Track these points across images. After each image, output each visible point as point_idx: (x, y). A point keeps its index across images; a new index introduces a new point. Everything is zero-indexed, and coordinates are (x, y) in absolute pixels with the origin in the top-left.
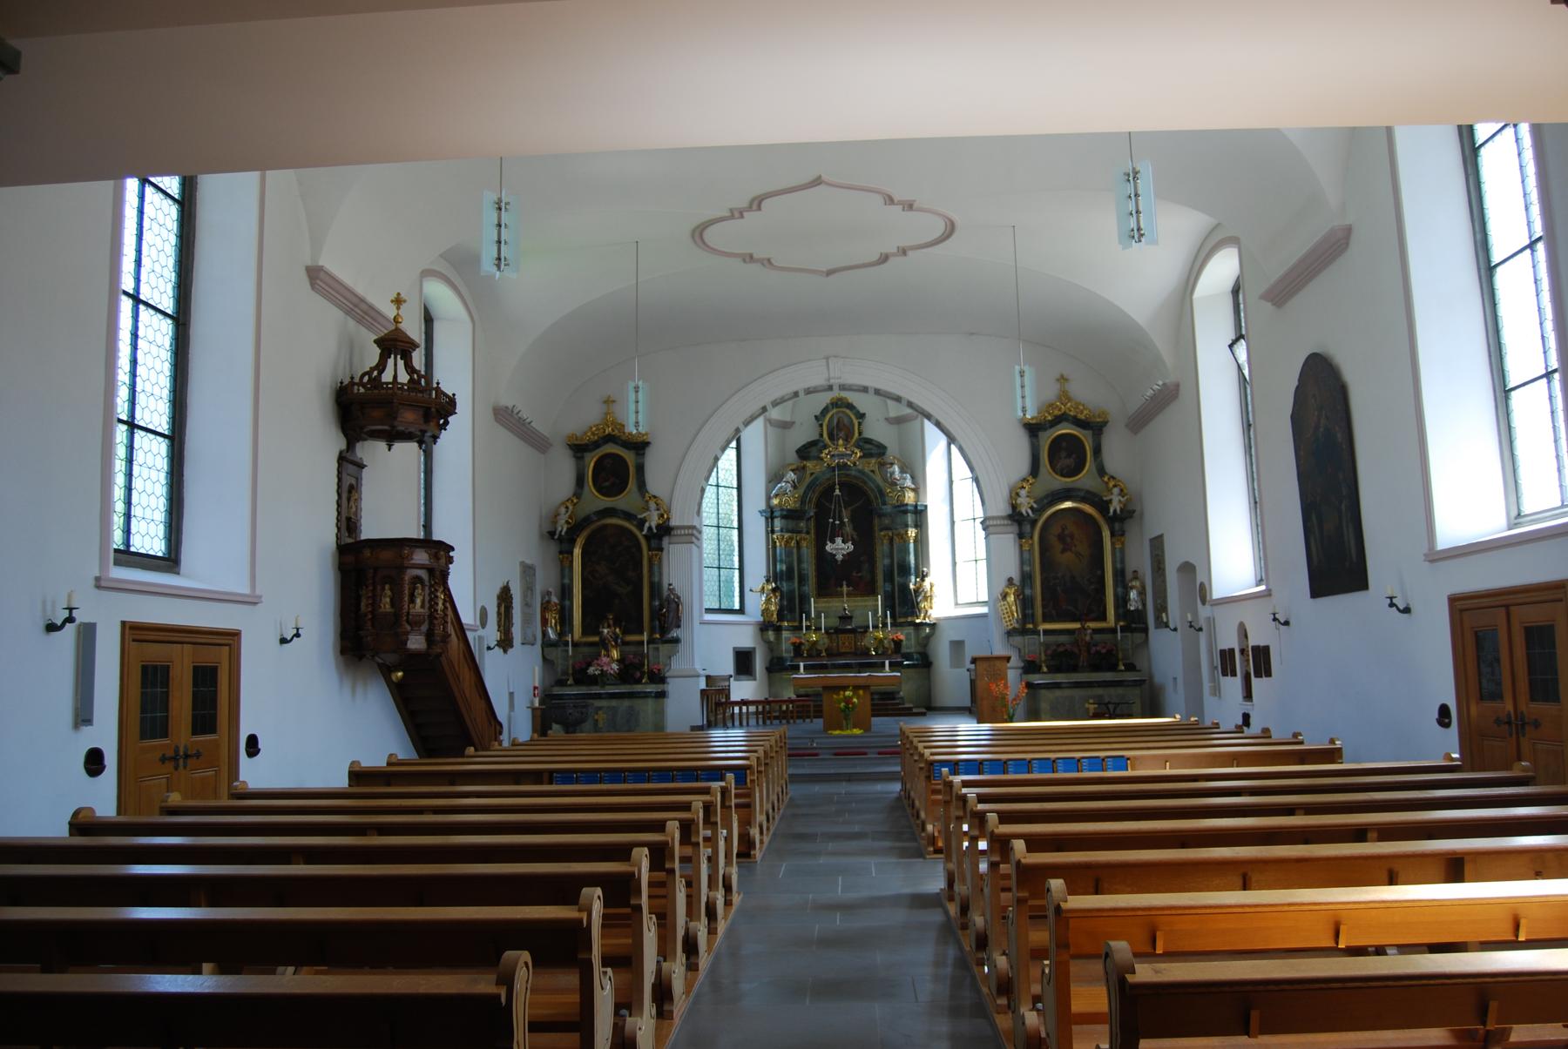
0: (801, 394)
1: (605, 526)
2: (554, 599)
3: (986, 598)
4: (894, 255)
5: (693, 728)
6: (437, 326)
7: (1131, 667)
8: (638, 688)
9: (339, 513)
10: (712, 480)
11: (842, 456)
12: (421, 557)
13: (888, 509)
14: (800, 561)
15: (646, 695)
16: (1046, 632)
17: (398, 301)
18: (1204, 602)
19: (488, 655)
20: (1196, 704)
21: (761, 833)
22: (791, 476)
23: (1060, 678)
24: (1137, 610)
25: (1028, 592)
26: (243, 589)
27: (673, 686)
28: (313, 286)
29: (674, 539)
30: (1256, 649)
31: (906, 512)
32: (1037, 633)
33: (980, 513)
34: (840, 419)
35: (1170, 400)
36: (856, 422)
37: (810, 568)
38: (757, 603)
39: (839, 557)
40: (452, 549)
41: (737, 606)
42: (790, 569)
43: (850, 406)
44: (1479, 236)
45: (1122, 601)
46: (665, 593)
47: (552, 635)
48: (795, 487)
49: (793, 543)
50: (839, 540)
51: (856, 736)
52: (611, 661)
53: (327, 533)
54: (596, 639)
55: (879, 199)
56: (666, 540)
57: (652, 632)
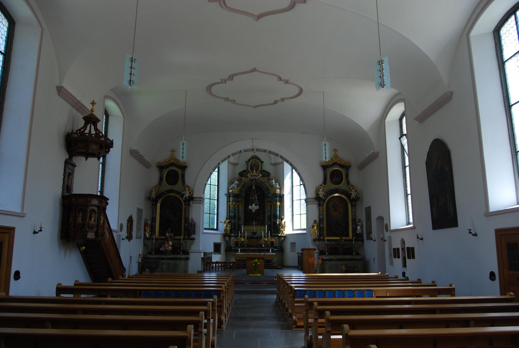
0: (243, 151)
1: (169, 196)
2: (149, 222)
3: (305, 228)
4: (279, 101)
5: (198, 272)
6: (111, 119)
7: (357, 254)
8: (179, 256)
9: (64, 183)
10: (209, 182)
11: (255, 176)
12: (95, 202)
13: (270, 195)
14: (238, 212)
15: (181, 259)
16: (328, 240)
17: (93, 103)
18: (387, 230)
19: (122, 242)
20: (383, 269)
21: (225, 317)
22: (237, 182)
23: (332, 257)
24: (360, 233)
25: (321, 225)
26: (18, 210)
27: (192, 256)
28: (59, 94)
29: (194, 202)
30: (408, 248)
31: (277, 196)
32: (324, 240)
33: (304, 197)
34: (255, 163)
35: (376, 158)
36: (260, 164)
37: (242, 215)
38: (222, 227)
39: (254, 211)
40: (108, 199)
41: (215, 228)
42: (235, 215)
43: (258, 159)
44: (505, 94)
45: (355, 230)
46: (190, 221)
47: (147, 235)
48: (238, 186)
49: (236, 206)
50: (254, 205)
51: (258, 277)
52: (169, 246)
53: (58, 190)
54: (164, 237)
55: (276, 78)
56: (191, 202)
57: (185, 235)
